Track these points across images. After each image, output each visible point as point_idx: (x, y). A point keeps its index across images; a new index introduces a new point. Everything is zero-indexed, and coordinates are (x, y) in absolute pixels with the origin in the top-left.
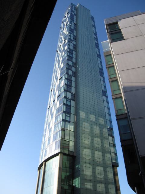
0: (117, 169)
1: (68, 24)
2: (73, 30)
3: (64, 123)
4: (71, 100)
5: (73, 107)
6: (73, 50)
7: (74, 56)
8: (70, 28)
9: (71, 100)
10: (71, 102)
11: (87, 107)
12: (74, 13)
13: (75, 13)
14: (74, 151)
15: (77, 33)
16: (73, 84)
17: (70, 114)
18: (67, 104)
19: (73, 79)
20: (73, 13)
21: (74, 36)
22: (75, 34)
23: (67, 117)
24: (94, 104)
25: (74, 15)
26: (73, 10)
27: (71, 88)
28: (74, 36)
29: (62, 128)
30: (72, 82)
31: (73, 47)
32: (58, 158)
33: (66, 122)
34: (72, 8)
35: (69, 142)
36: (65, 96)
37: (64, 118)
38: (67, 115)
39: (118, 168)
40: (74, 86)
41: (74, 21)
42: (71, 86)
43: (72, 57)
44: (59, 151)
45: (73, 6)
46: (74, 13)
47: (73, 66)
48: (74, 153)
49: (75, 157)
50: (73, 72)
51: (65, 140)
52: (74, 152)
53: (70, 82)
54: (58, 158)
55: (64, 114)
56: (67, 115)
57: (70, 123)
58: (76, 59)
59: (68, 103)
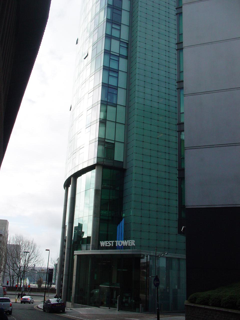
0: (183, 316)
3: (108, 41)
5: (123, 90)
14: (123, 161)
16: (125, 18)
17: (119, 24)
23: (111, 79)
24: (167, 18)
27: (118, 28)
29: (108, 4)
30: (123, 12)
32: (92, 175)
33: (113, 40)
35: (114, 144)
36: (109, 3)
37: (109, 33)
38: (111, 58)
39: (184, 317)
42: (120, 10)
44: (96, 162)
48: (123, 164)
49: (125, 170)
52: (123, 162)
53: (118, 12)
54: (92, 175)
55: (109, 25)
56: (114, 26)
59: (114, 65)
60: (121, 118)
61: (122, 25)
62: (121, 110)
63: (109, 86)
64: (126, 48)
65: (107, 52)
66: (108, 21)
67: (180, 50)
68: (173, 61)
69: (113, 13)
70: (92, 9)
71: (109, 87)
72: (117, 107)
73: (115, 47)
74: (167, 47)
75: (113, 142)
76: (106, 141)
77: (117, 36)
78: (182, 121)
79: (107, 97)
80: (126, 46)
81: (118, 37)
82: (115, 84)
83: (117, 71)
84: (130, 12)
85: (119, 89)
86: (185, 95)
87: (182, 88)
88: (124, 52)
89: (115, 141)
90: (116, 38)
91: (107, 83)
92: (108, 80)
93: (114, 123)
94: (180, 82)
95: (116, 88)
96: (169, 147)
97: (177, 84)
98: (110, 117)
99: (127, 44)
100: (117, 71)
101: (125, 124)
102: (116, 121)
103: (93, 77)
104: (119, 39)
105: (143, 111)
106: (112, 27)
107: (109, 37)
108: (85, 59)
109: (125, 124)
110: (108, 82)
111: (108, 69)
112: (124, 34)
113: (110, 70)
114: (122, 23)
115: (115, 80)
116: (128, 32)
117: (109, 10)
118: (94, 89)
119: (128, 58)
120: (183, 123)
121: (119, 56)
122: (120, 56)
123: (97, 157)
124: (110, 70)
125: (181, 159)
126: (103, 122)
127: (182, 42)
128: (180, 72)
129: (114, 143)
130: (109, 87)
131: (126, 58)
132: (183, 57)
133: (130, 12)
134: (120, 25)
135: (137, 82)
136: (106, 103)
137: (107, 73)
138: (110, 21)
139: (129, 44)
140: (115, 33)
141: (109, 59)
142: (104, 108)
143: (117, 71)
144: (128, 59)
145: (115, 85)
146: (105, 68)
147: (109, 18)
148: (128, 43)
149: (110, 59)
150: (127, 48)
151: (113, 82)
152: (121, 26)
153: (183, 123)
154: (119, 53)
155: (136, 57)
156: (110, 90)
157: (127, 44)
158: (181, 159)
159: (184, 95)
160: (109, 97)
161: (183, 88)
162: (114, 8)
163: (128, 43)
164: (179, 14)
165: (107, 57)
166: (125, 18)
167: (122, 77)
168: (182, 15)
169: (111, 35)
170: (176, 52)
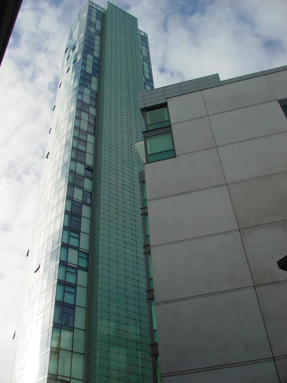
1: (78, 60)
2: (91, 76)
3: (64, 250)
4: (77, 269)
6: (90, 105)
7: (90, 149)
8: (83, 71)
9: (77, 269)
10: (77, 274)
11: (130, 108)
12: (95, 28)
13: (98, 27)
15: (99, 85)
16: (85, 226)
17: (78, 232)
18: (71, 243)
19: (86, 211)
20: (93, 30)
21: (94, 58)
22: (94, 87)
23: (67, 295)
25: (96, 34)
26: (94, 19)
27: (77, 236)
28: (94, 58)
30: (77, 309)
31: (91, 97)
33: (70, 250)
34: (89, 15)
37: (65, 241)
38: (66, 289)
40: (89, 217)
41: (93, 50)
42: (80, 216)
43: (85, 152)
45: (93, 10)
46: (95, 28)
47: (85, 177)
50: (85, 193)
51: (75, 173)
55: (66, 233)
56: (71, 234)
57: (73, 331)
58: (96, 156)
59: (70, 279)
60: (80, 347)
61: (81, 234)
62: (80, 335)
63: (64, 304)
64: (86, 259)
65: (63, 264)
66: (65, 228)
67: (147, 253)
68: (140, 225)
69: (70, 220)
70: (47, 216)
71: (71, 231)
72: (73, 331)
73: (73, 257)
74: (132, 205)
75: (68, 380)
76: (59, 378)
77: (76, 245)
78: (156, 341)
79: (61, 318)
80: (86, 257)
81: (77, 246)
82: (72, 302)
83: (74, 286)
84: (90, 219)
85: (77, 308)
86: (158, 304)
87: (150, 252)
88: (83, 263)
89: (70, 378)
90: (73, 247)
91: (64, 280)
92: (75, 167)
93: (70, 353)
94: (150, 291)
95: (73, 307)
96: (140, 321)
97: (146, 294)
98: (65, 344)
99: (88, 254)
100: (74, 286)
101: (84, 354)
102: (72, 350)
103: (44, 294)
104: (77, 248)
105: (107, 328)
106: (70, 236)
107: (65, 246)
108: (35, 272)
109: (84, 354)
110: (75, 169)
111: (62, 304)
112: (84, 243)
113: (65, 285)
114: (77, 284)
115: (77, 241)
116: (87, 281)
117: (67, 216)
118: (56, 218)
119: (92, 206)
120: (157, 344)
121: (77, 268)
122: (79, 268)
123: (48, 373)
124: (65, 285)
125: (144, 200)
126: (56, 352)
127: (148, 235)
128: (150, 280)
129: (70, 381)
130: (71, 231)
131: (86, 270)
132: (148, 223)
133: (90, 219)
134: (74, 308)
135: (99, 299)
136: (73, 185)
137: (61, 288)
138: (69, 213)
139: (90, 257)
140: (73, 242)
141: (65, 271)
142: (56, 335)
143: (74, 286)
144: (88, 272)
145: (72, 303)
146: (60, 283)
147: (69, 210)
148: (89, 254)
149: (66, 271)
150: (88, 259)
151: (69, 299)
152: (76, 288)
153: (157, 344)
154: (77, 265)
155: (97, 341)
156: (66, 309)
157: (88, 254)
158: (144, 200)
159: (157, 304)
160: (64, 318)
161: (158, 354)
162: (65, 306)
163: (88, 253)
164: (145, 214)
165: (63, 269)
166: (85, 226)
167: (81, 293)
168: (151, 254)
169: (63, 302)
170: (144, 255)
